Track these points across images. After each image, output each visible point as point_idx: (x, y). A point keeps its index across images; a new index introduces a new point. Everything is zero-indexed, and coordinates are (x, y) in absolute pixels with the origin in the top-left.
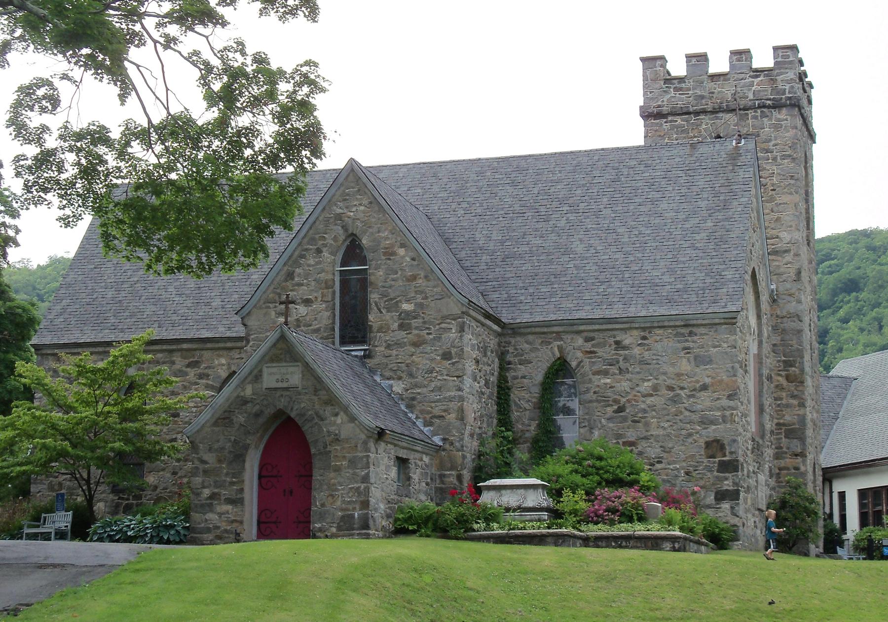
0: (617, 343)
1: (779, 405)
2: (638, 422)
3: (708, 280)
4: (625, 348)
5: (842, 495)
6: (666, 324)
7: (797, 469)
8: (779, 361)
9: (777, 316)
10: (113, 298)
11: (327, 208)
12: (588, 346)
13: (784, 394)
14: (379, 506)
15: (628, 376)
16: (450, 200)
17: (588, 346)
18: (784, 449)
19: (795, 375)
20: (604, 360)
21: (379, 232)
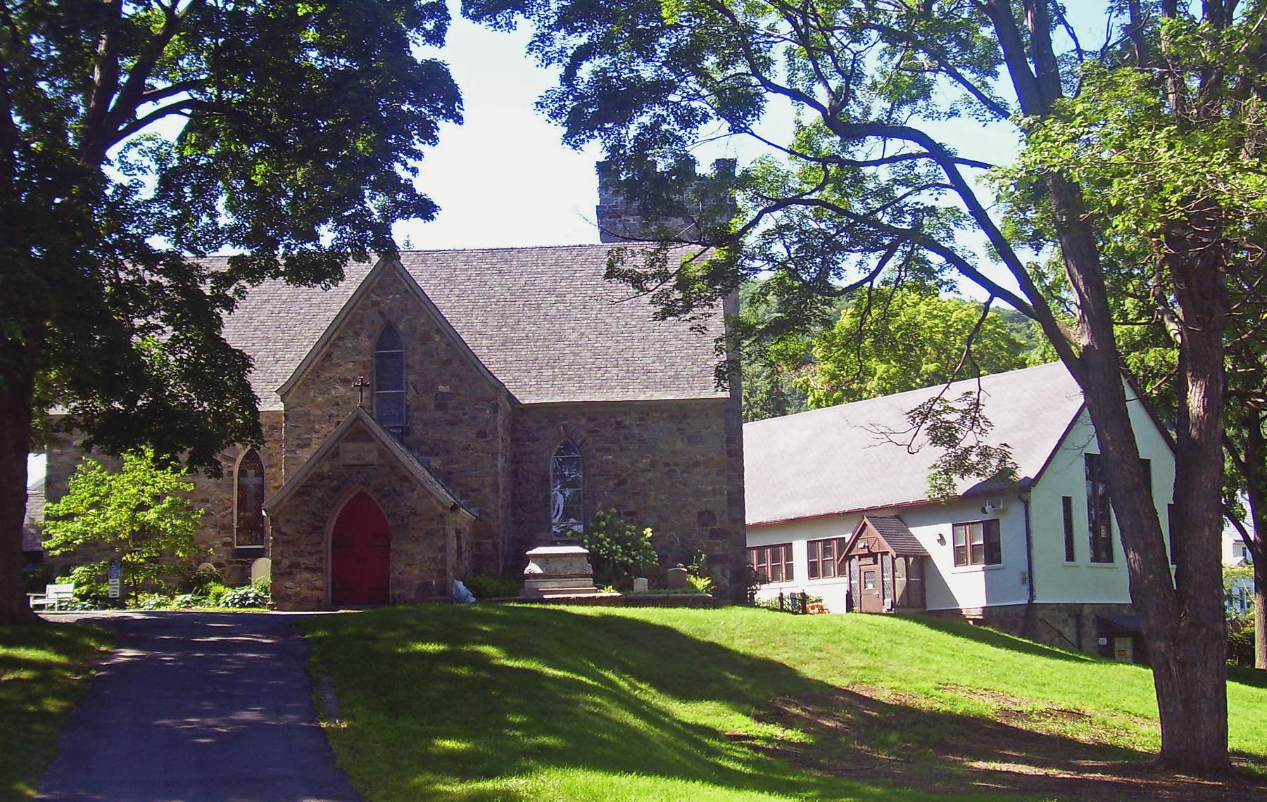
3: (696, 369)
12: (591, 425)
17: (591, 425)
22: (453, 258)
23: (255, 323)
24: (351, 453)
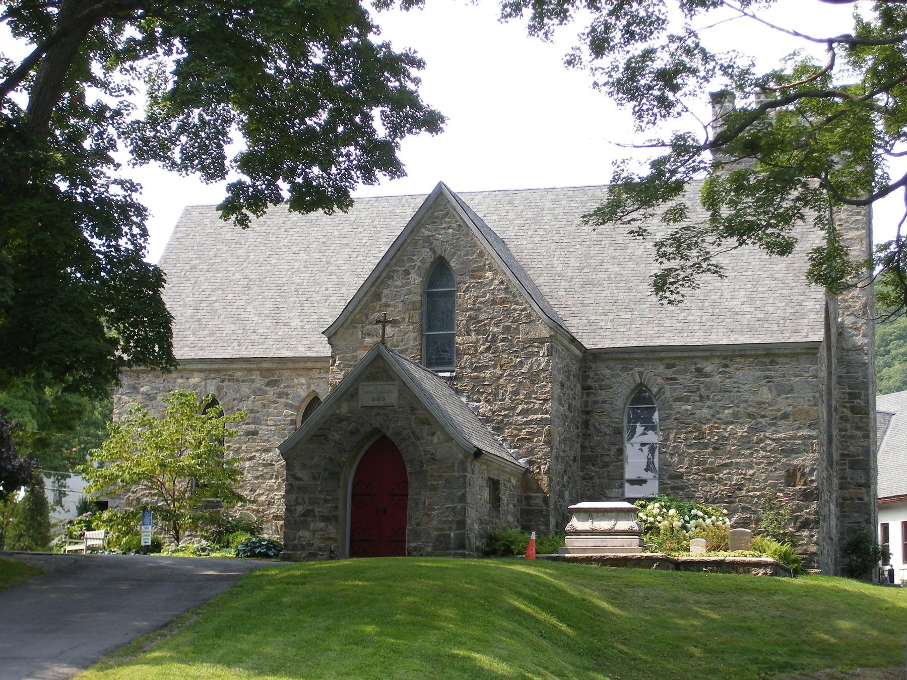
0: (699, 370)
1: (843, 436)
2: (718, 449)
3: (789, 310)
4: (707, 376)
5: (886, 527)
6: (748, 352)
7: (861, 499)
8: (844, 393)
9: (843, 349)
10: (192, 317)
11: (415, 230)
12: (669, 373)
13: (849, 426)
14: (474, 528)
15: (709, 403)
16: (527, 226)
17: (669, 373)
18: (849, 480)
19: (860, 407)
20: (685, 387)
21: (467, 255)
22: (541, 198)
23: (332, 268)
24: (368, 395)
